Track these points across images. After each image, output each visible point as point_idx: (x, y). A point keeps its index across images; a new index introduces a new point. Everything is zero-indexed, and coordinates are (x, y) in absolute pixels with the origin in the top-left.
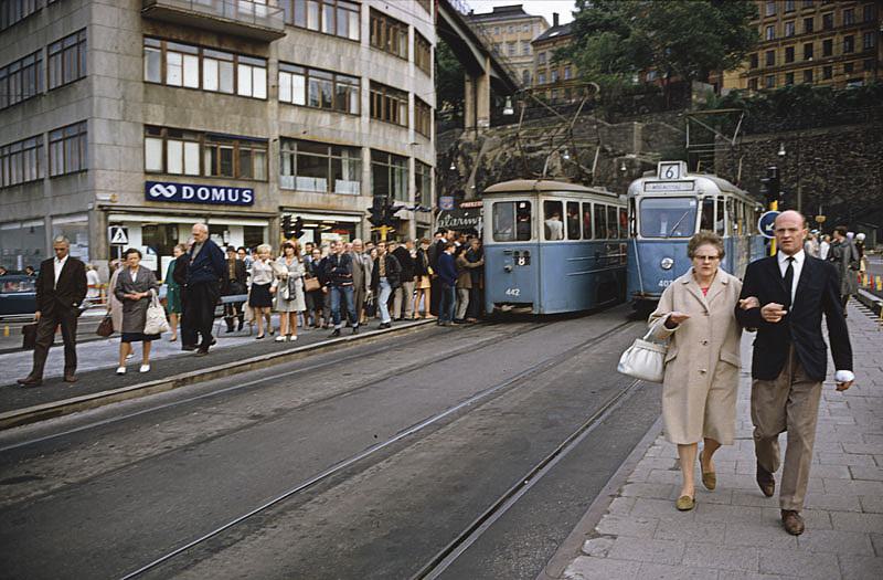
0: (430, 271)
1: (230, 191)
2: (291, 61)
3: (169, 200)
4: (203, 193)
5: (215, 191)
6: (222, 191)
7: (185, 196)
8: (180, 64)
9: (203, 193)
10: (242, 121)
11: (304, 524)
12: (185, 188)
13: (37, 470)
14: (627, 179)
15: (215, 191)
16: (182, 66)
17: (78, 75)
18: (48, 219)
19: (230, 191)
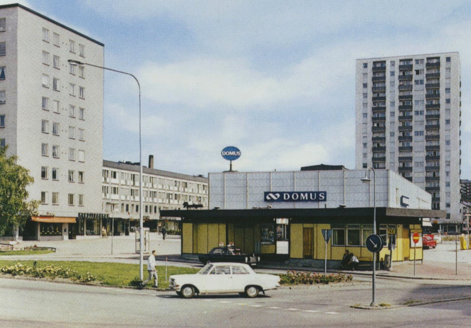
0: (291, 219)
1: (311, 195)
2: (142, 148)
3: (277, 201)
4: (295, 196)
5: (302, 195)
6: (306, 195)
7: (285, 198)
8: (398, 260)
9: (295, 196)
10: (38, 267)
11: (339, 198)
12: (285, 195)
13: (236, 239)
14: (226, 252)
15: (302, 195)
16: (397, 261)
17: (265, 290)
18: (120, 185)
19: (311, 195)
